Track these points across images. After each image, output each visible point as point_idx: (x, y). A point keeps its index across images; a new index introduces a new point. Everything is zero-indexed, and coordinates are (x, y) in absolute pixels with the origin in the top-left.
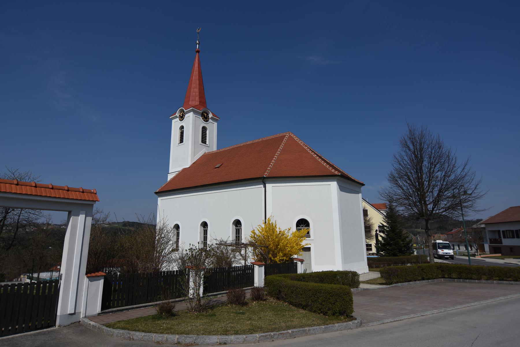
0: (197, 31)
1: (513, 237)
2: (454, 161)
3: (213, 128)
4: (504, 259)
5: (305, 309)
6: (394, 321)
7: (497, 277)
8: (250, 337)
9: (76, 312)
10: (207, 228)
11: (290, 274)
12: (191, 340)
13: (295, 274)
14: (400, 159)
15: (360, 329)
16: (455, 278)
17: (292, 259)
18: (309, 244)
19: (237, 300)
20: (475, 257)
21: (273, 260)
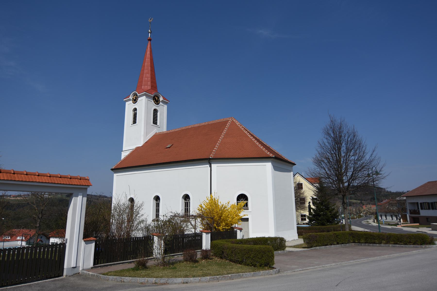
0: (149, 21)
1: (429, 209)
2: (364, 148)
3: (163, 110)
4: (418, 228)
5: (242, 264)
6: (303, 270)
7: (392, 241)
8: (203, 279)
9: (77, 266)
10: (160, 201)
11: (231, 239)
12: (164, 281)
13: (235, 240)
14: (323, 145)
15: (277, 275)
16: (363, 243)
17: (233, 228)
18: (246, 215)
19: (191, 259)
20: (397, 226)
21: (217, 229)
